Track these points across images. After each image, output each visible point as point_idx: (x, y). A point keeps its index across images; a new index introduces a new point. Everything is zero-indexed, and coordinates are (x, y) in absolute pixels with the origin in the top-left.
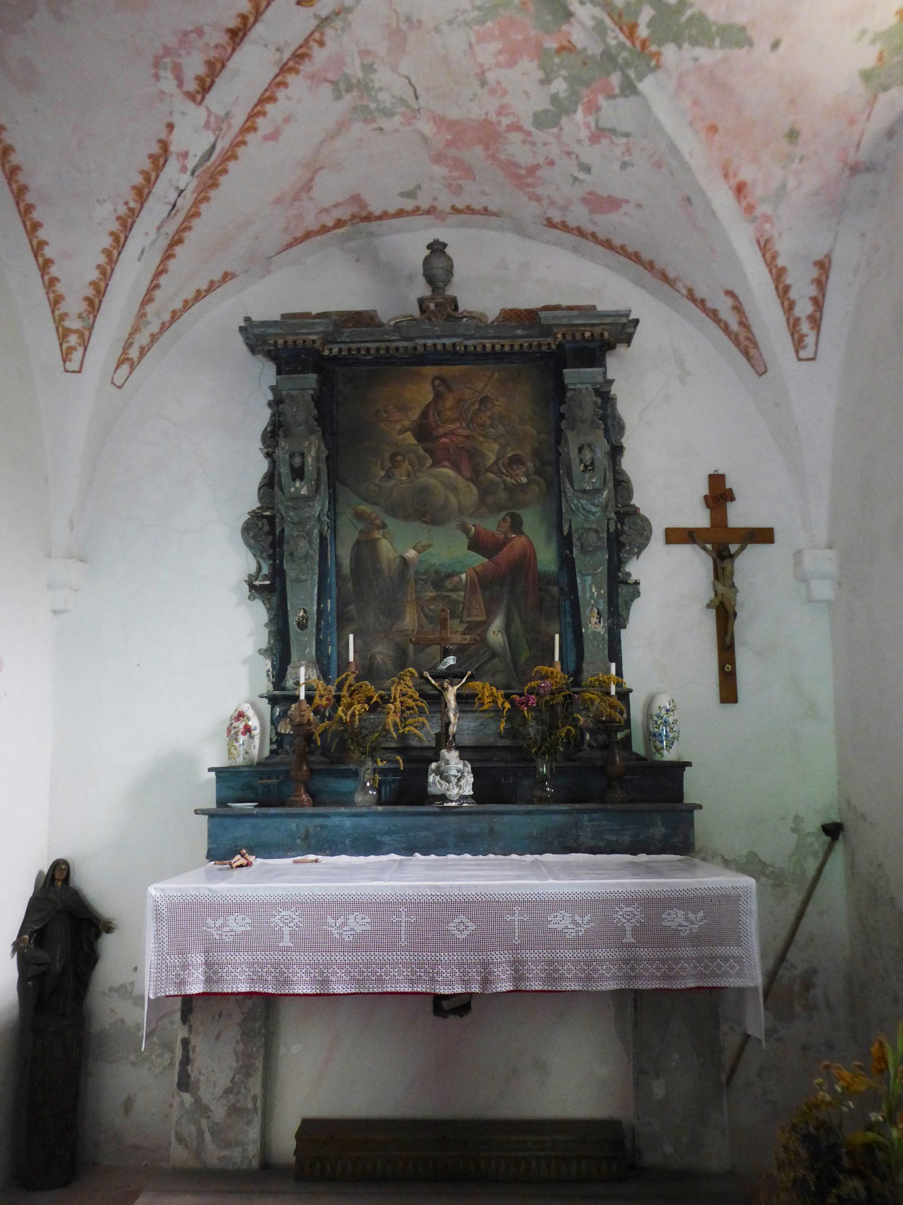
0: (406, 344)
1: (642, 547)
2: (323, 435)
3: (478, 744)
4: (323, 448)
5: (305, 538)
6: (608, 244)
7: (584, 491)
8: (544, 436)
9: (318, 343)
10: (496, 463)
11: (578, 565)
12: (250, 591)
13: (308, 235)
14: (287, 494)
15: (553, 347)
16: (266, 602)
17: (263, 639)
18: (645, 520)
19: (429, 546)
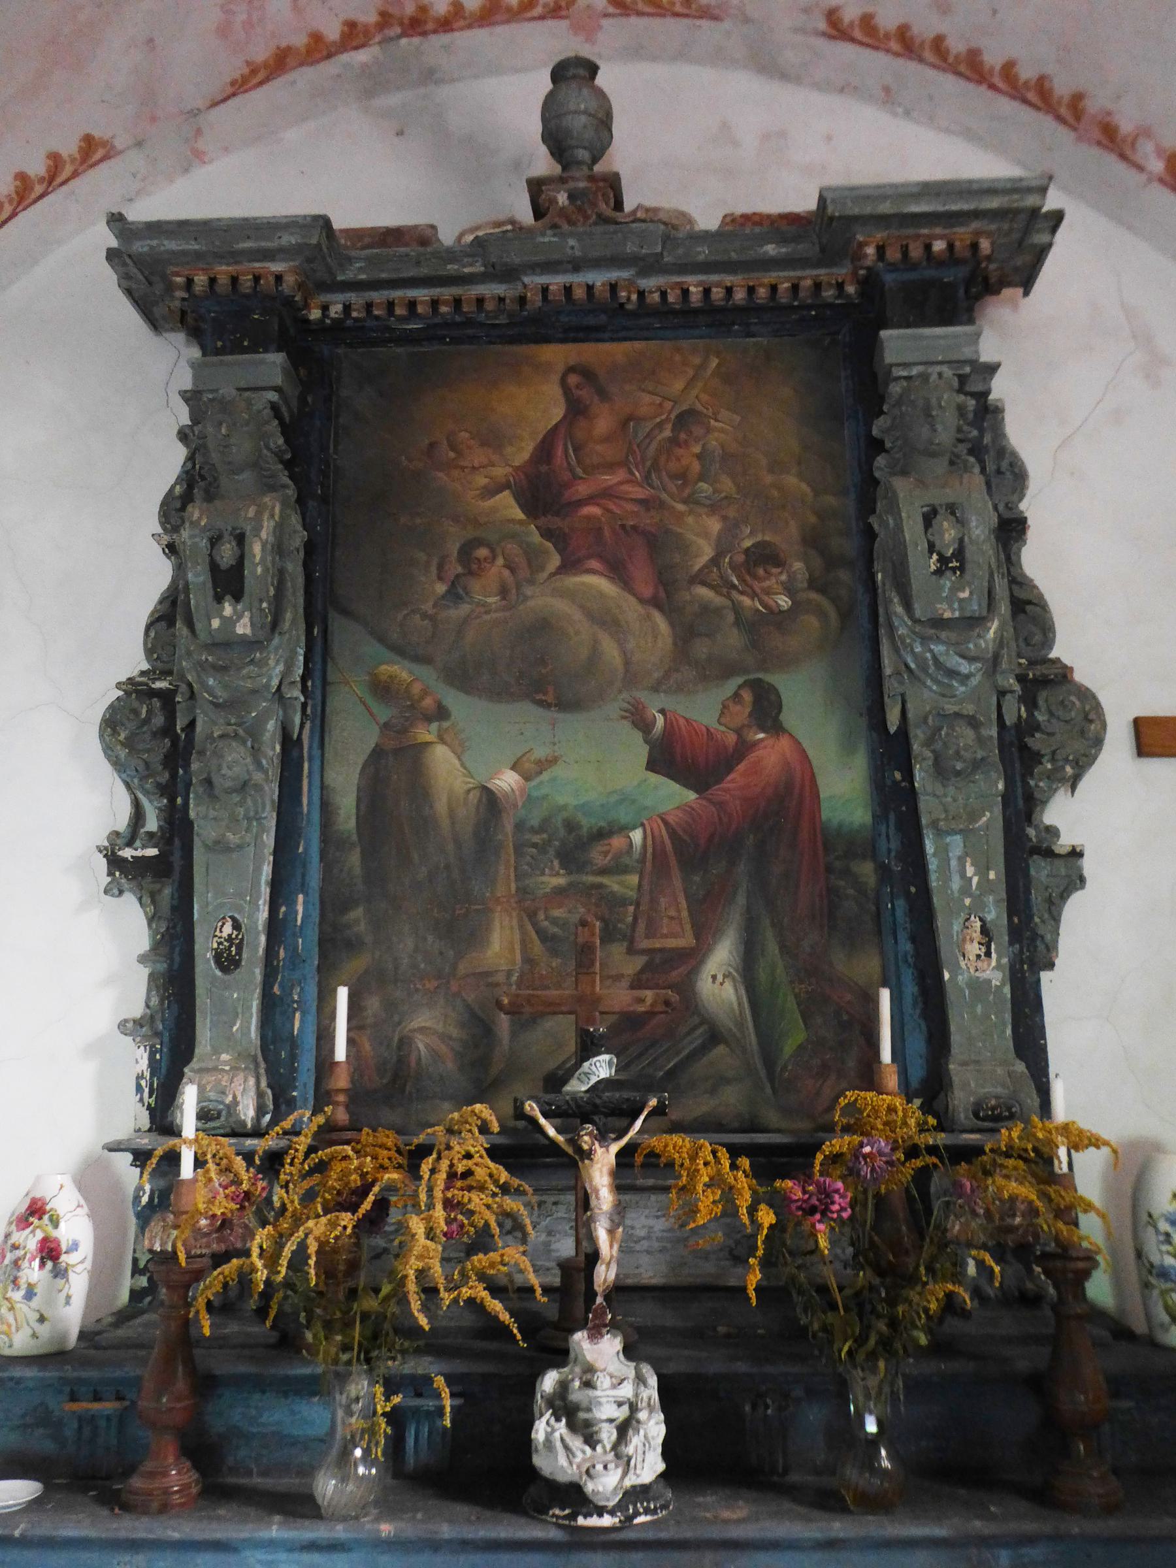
0: (499, 289)
1: (1083, 763)
2: (301, 501)
3: (672, 1281)
4: (295, 520)
5: (244, 743)
6: (972, 68)
7: (939, 623)
8: (830, 500)
9: (290, 280)
10: (715, 561)
11: (928, 807)
12: (110, 874)
13: (280, 62)
14: (203, 636)
15: (851, 289)
16: (147, 900)
17: (134, 993)
18: (1087, 695)
19: (552, 761)
